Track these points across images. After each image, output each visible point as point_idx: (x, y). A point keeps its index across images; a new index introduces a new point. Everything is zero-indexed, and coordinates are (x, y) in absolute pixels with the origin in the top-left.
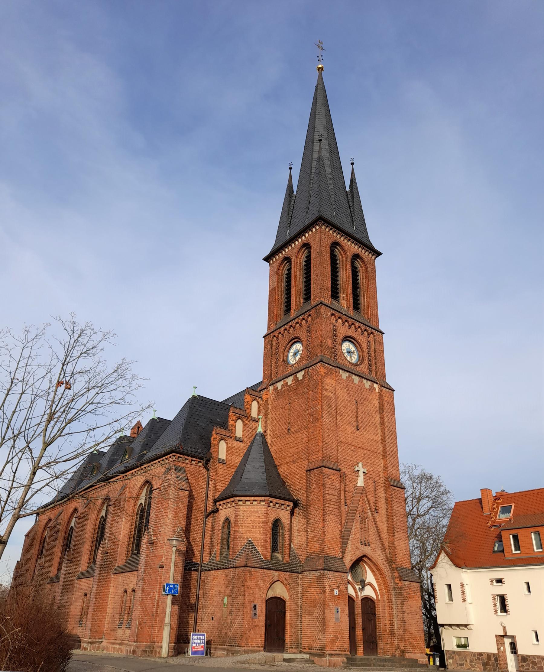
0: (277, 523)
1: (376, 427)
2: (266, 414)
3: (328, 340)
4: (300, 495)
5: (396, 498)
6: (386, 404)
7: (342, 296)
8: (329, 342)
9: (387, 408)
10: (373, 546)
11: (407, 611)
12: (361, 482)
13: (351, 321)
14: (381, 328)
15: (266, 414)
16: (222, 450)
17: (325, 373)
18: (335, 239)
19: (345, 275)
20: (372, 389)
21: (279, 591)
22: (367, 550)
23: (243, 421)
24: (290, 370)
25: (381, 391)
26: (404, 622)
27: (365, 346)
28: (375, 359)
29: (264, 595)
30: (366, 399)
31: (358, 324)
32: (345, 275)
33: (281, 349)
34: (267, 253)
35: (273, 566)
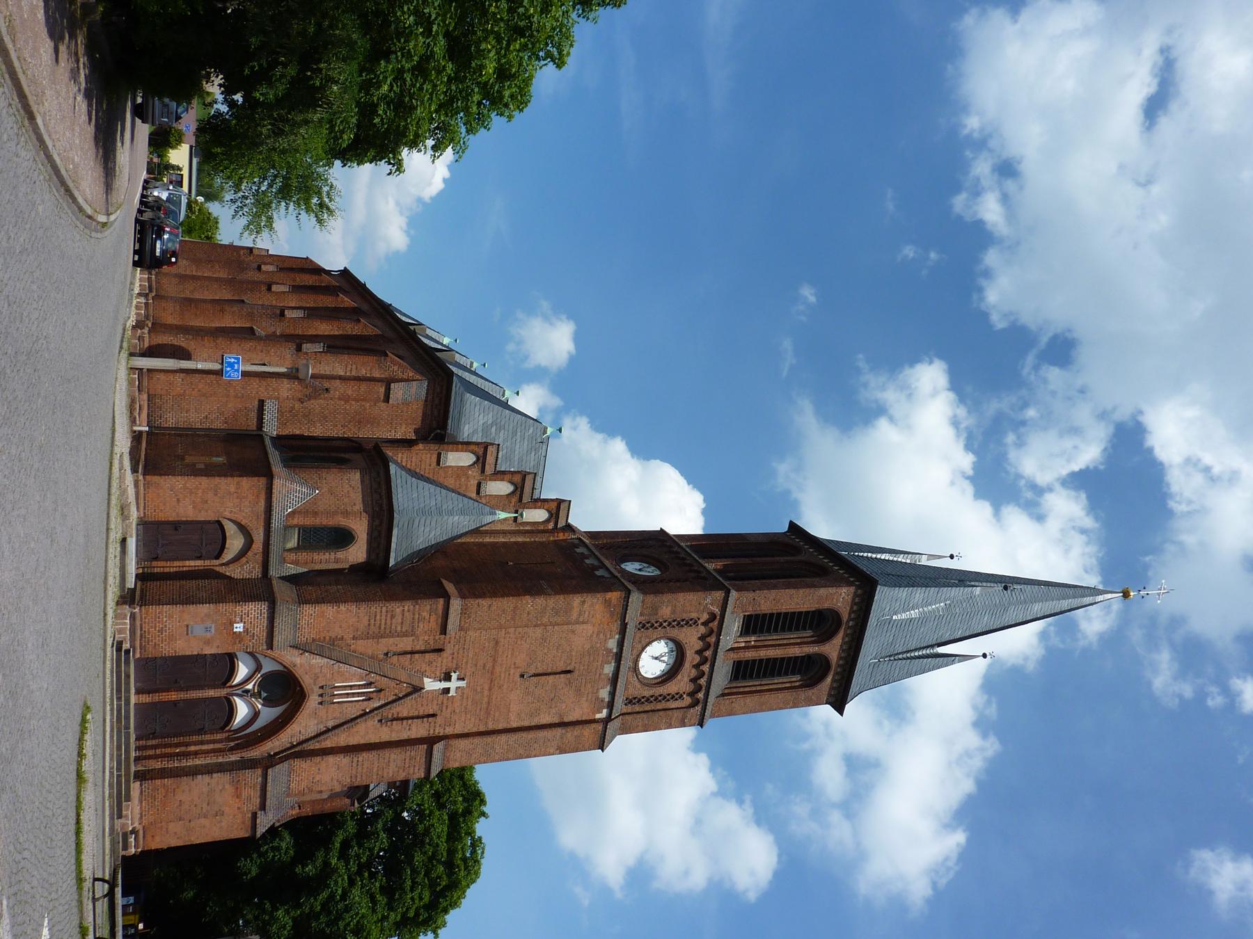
9: (571, 734)
10: (322, 711)
14: (710, 723)
22: (312, 701)
23: (513, 493)
27: (672, 688)
29: (227, 514)
30: (578, 691)
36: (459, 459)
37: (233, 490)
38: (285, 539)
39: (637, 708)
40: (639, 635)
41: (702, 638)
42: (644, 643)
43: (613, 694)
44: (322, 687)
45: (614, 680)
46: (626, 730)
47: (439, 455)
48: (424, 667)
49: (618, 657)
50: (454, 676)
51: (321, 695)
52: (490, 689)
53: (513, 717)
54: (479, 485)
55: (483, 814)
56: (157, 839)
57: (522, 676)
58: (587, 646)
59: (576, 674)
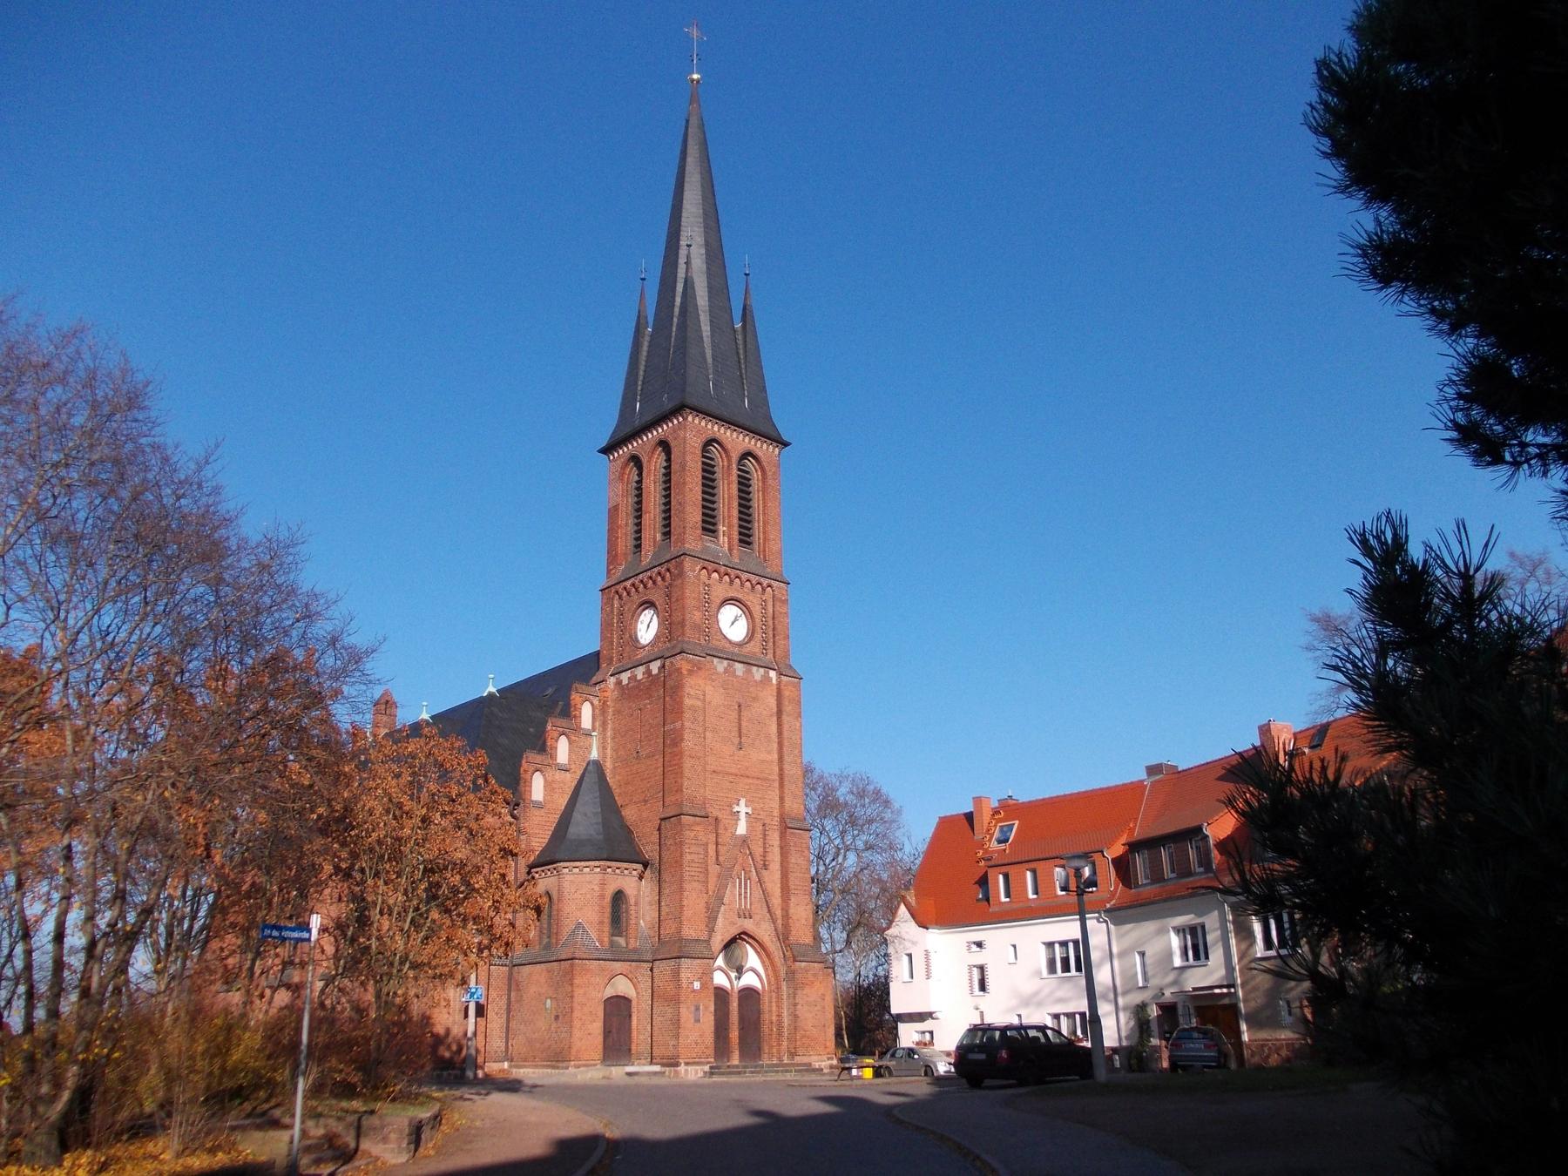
0: (619, 897)
2: (604, 724)
4: (650, 851)
7: (722, 528)
12: (742, 829)
13: (733, 573)
15: (604, 724)
16: (537, 788)
18: (710, 435)
19: (727, 491)
20: (767, 679)
21: (623, 987)
22: (748, 925)
24: (641, 654)
25: (779, 683)
26: (796, 1016)
27: (757, 610)
30: (755, 699)
31: (745, 576)
32: (727, 491)
33: (628, 615)
34: (604, 444)
35: (616, 955)
53: (769, 758)
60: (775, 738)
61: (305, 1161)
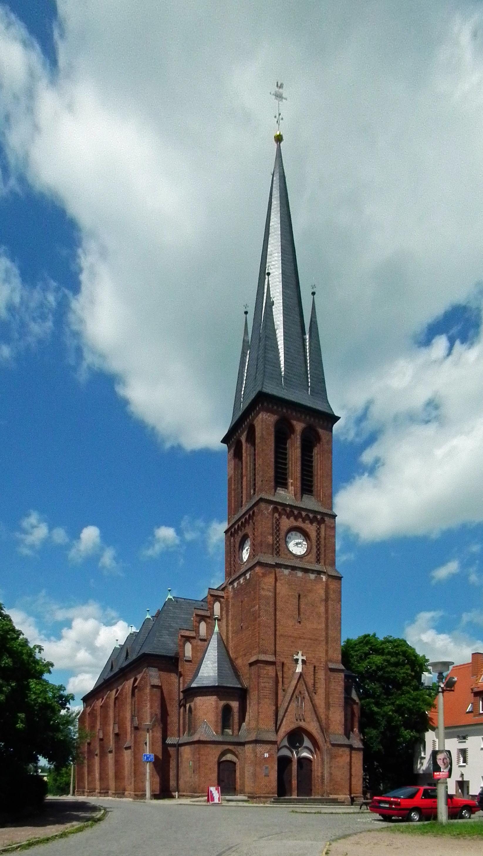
1: (319, 617)
3: (269, 537)
5: (334, 679)
6: (331, 593)
7: (290, 481)
8: (270, 539)
10: (308, 720)
11: (333, 766)
15: (227, 612)
17: (262, 573)
22: (302, 724)
23: (205, 621)
25: (327, 581)
27: (313, 535)
28: (325, 546)
30: (310, 591)
36: (188, 650)
37: (205, 758)
38: (227, 735)
39: (322, 556)
40: (283, 555)
41: (288, 518)
42: (287, 552)
43: (313, 571)
44: (297, 720)
45: (306, 571)
46: (333, 563)
47: (187, 661)
48: (291, 672)
49: (294, 568)
50: (296, 657)
51: (300, 720)
52: (304, 639)
53: (319, 627)
54: (202, 640)
55: (374, 635)
56: (358, 789)
57: (300, 622)
58: (287, 586)
59: (301, 593)
60: (323, 615)
61: (417, 735)
